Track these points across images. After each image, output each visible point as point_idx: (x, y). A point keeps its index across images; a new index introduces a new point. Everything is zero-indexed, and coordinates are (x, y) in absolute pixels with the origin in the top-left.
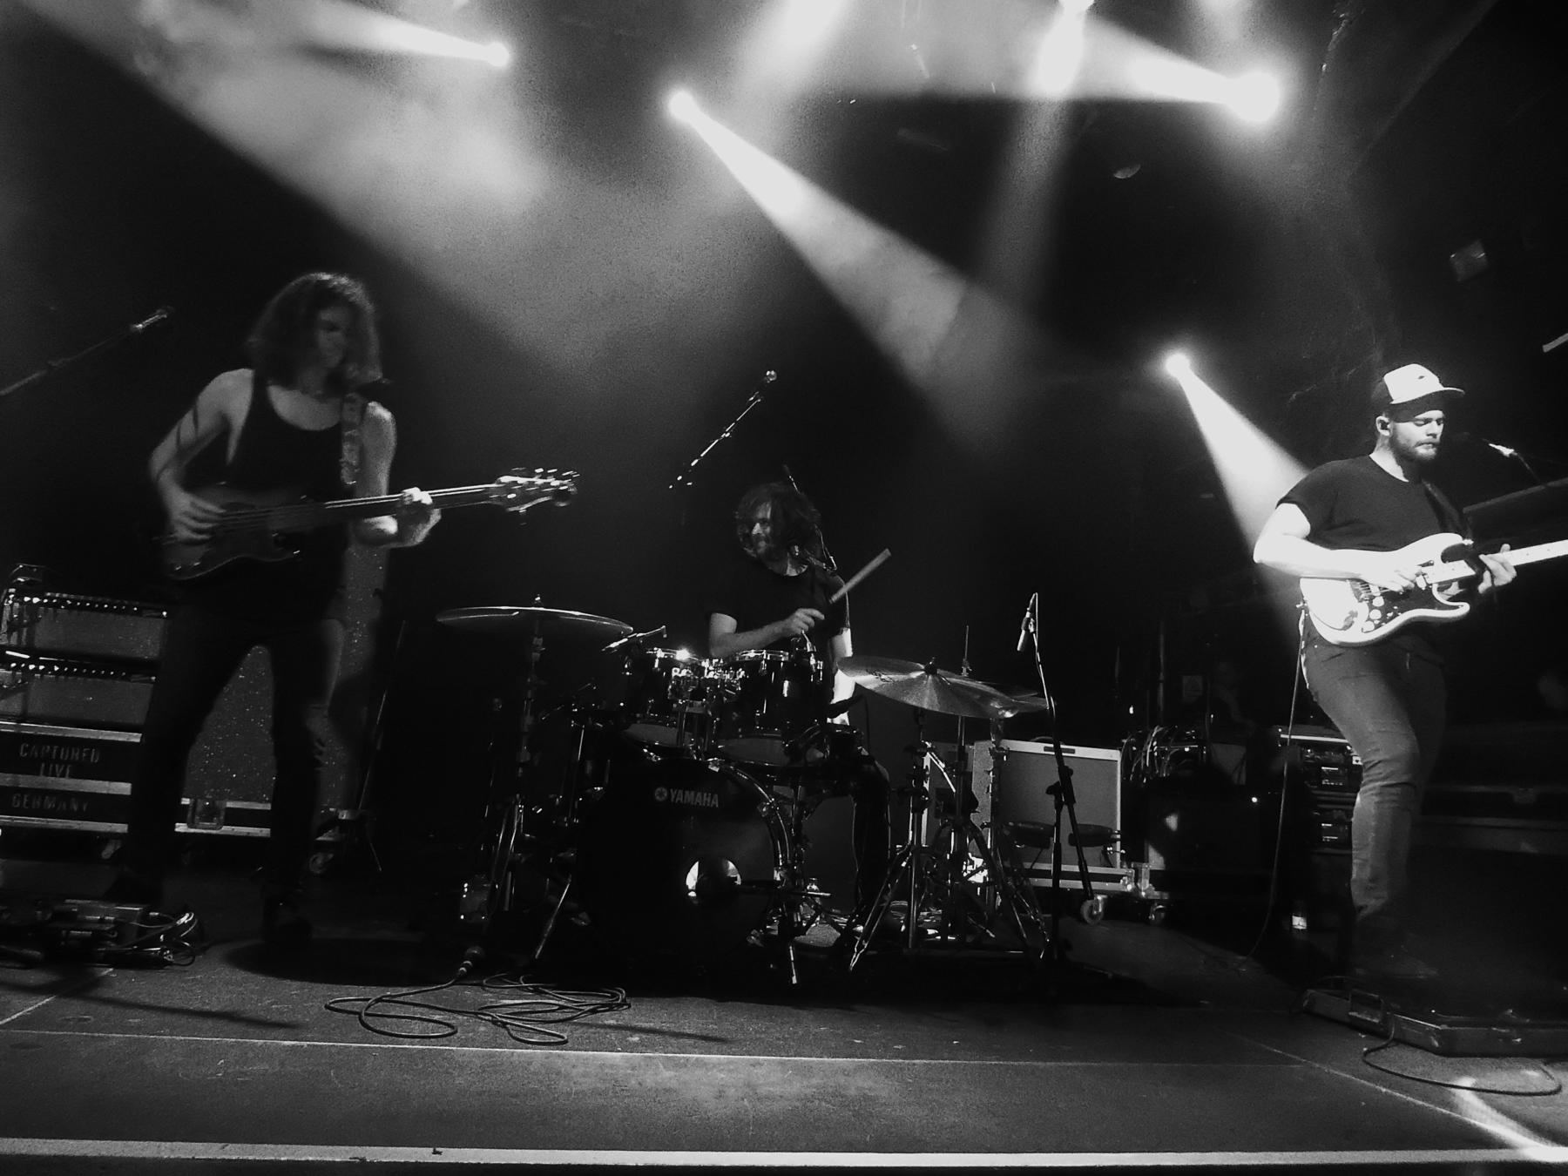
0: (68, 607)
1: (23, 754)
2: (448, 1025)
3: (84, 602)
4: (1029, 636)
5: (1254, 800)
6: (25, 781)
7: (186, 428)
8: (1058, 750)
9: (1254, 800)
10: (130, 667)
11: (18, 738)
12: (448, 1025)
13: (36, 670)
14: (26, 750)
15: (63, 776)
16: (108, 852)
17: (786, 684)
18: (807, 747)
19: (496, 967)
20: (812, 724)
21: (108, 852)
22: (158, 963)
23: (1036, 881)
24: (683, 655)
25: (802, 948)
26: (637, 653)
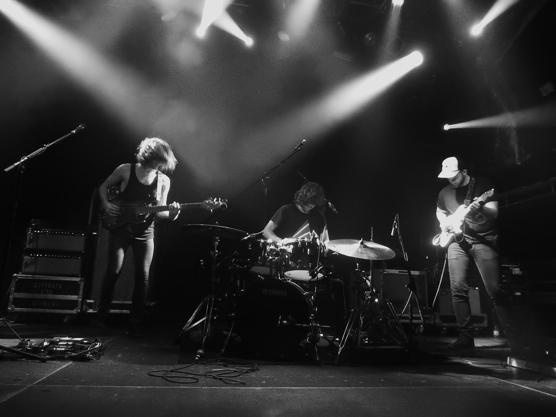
1: (35, 287)
2: (195, 379)
3: (61, 232)
4: (396, 230)
5: (547, 353)
6: (36, 296)
7: (111, 178)
9: (547, 353)
10: (74, 254)
11: (33, 281)
12: (195, 379)
15: (49, 294)
16: (65, 320)
17: (308, 250)
18: (318, 273)
21: (65, 320)
25: (318, 347)
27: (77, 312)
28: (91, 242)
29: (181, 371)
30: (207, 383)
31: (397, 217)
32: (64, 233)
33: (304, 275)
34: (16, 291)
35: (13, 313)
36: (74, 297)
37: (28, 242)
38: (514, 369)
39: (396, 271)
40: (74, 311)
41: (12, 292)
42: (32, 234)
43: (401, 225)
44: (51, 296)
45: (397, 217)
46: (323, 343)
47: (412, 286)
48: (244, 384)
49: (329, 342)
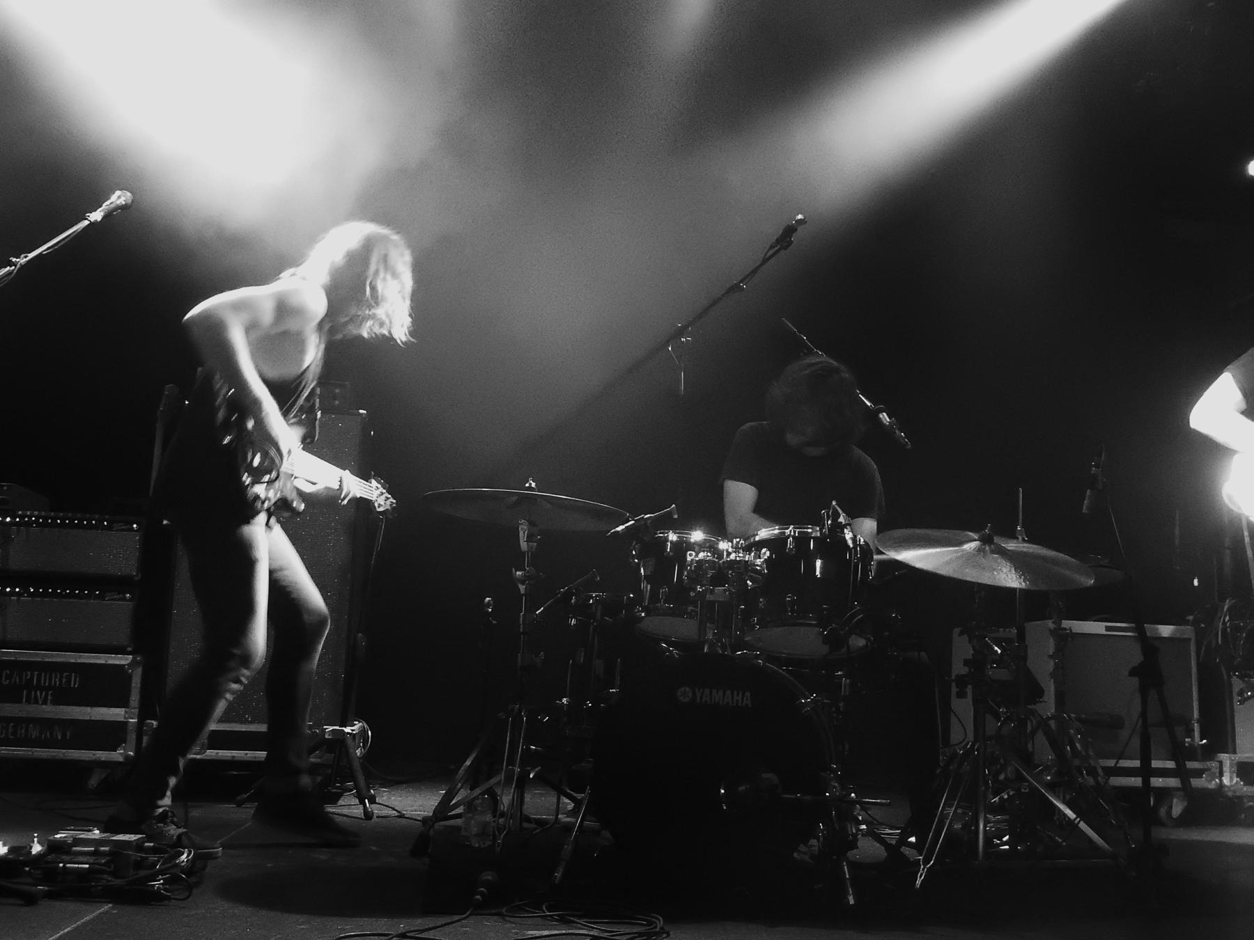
0: (39, 525)
13: (13, 593)
14: (9, 677)
15: (45, 702)
16: (93, 782)
17: (819, 563)
20: (853, 607)
21: (93, 782)
22: (30, 900)
24: (697, 536)
25: (854, 866)
27: (127, 757)
36: (115, 714)
40: (117, 755)
46: (867, 849)
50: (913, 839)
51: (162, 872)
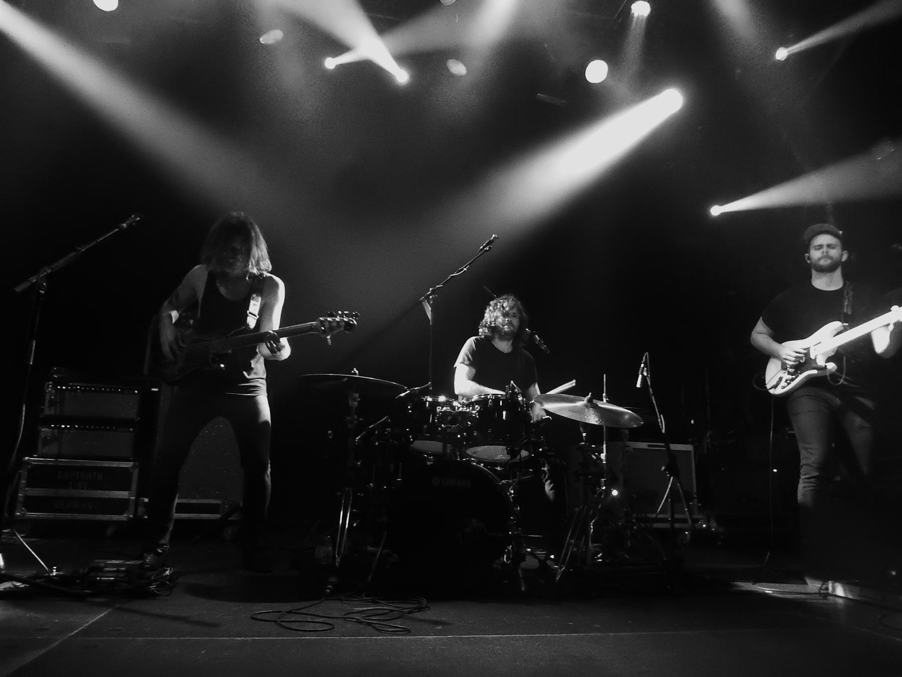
3: (101, 388)
4: (644, 378)
6: (63, 492)
8: (668, 448)
9: (894, 573)
10: (127, 423)
13: (66, 427)
16: (110, 532)
17: (504, 413)
19: (347, 589)
21: (110, 532)
22: (152, 596)
23: (656, 525)
24: (442, 399)
25: (524, 570)
26: (416, 400)
27: (129, 518)
28: (148, 403)
29: (304, 611)
30: (344, 631)
31: (646, 356)
32: (106, 389)
33: (499, 453)
34: (30, 484)
35: (24, 521)
36: (123, 494)
37: (47, 404)
38: (840, 601)
39: (643, 445)
40: (123, 517)
41: (21, 486)
42: (53, 391)
43: (651, 371)
44: (86, 493)
45: (646, 356)
46: (530, 563)
47: (673, 469)
48: (407, 632)
49: (540, 560)
50: (552, 557)
51: (155, 581)
